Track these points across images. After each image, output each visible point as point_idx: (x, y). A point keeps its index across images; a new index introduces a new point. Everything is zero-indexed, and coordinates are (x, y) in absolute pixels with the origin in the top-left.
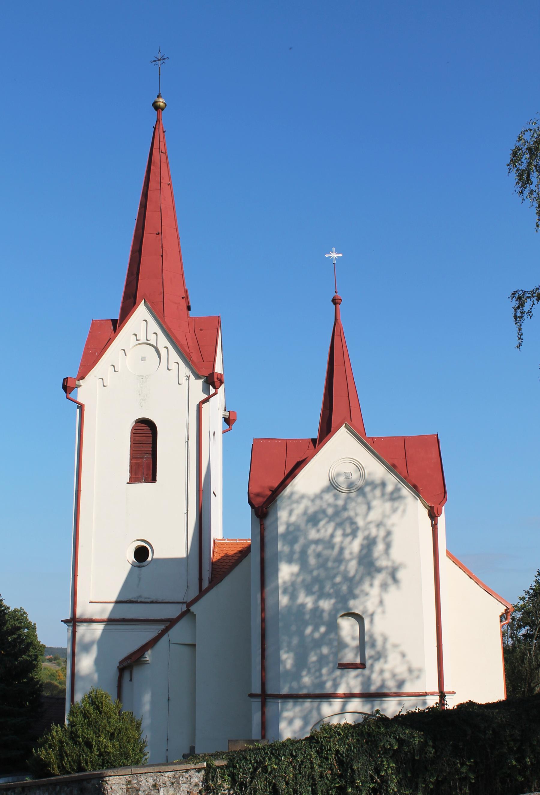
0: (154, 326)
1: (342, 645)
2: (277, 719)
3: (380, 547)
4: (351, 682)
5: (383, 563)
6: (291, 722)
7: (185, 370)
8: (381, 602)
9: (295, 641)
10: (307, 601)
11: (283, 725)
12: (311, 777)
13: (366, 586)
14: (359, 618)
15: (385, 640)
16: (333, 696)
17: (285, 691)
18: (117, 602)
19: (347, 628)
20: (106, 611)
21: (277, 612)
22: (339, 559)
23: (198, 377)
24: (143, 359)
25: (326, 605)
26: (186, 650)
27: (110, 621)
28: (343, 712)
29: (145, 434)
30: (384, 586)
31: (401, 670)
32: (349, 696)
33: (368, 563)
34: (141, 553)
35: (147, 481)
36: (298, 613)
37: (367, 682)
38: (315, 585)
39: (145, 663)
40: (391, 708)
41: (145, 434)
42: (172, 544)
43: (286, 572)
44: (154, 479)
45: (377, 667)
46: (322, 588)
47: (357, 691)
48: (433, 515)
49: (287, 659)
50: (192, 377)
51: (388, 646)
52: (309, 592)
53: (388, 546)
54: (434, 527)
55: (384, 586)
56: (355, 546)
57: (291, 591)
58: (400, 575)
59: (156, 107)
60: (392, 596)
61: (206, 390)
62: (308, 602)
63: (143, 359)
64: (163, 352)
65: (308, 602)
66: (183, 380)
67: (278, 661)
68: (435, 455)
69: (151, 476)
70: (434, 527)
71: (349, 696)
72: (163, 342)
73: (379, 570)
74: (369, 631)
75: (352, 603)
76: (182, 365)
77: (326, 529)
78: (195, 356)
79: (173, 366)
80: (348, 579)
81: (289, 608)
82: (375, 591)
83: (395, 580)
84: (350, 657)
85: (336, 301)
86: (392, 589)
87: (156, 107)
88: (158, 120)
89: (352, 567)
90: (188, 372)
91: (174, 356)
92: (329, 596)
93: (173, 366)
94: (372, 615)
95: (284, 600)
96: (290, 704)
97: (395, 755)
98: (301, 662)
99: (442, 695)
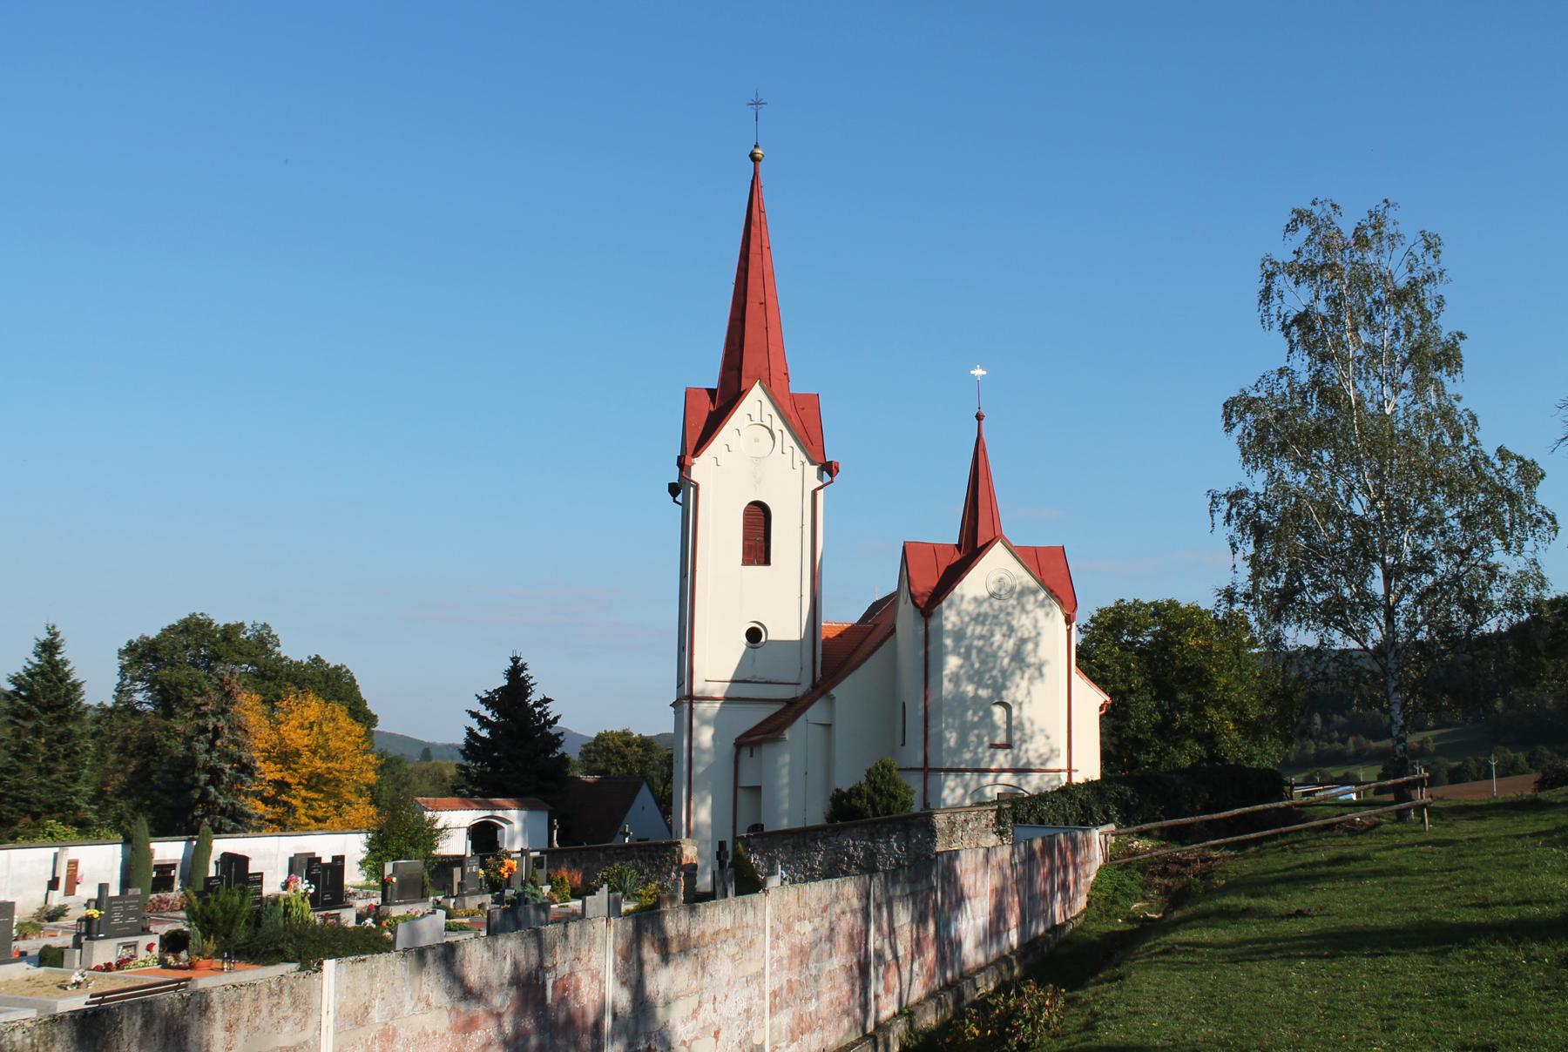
0: (768, 408)
1: (994, 727)
2: (940, 788)
3: (1030, 646)
4: (1002, 759)
5: (1031, 659)
6: (953, 790)
7: (800, 456)
8: (1029, 693)
9: (957, 723)
11: (946, 793)
12: (1064, 816)
13: (1017, 678)
14: (1007, 707)
15: (1032, 724)
16: (988, 771)
17: (948, 765)
18: (732, 681)
19: (999, 713)
20: (719, 690)
22: (994, 655)
23: (813, 463)
24: (757, 441)
25: (983, 693)
26: (820, 729)
27: (727, 699)
28: (995, 783)
29: (758, 519)
30: (1031, 679)
31: (1044, 750)
32: (1002, 771)
33: (1018, 657)
34: (754, 635)
35: (759, 564)
36: (960, 700)
37: (1016, 759)
38: (977, 678)
39: (783, 740)
40: (1033, 784)
41: (758, 519)
42: (786, 626)
43: (953, 663)
44: (767, 562)
45: (1024, 747)
46: (981, 679)
47: (1006, 766)
48: (1069, 621)
49: (952, 738)
50: (807, 463)
51: (1036, 728)
52: (970, 679)
53: (1037, 645)
54: (1069, 631)
55: (1031, 679)
56: (1010, 645)
57: (956, 679)
58: (1045, 670)
59: (754, 158)
60: (1038, 687)
61: (820, 477)
62: (970, 689)
63: (757, 441)
64: (778, 435)
65: (970, 689)
66: (798, 465)
67: (941, 739)
68: (1063, 564)
70: (1069, 631)
71: (1002, 771)
72: (778, 425)
73: (1029, 666)
74: (1019, 717)
75: (1004, 693)
76: (797, 449)
79: (788, 450)
80: (1003, 672)
82: (1024, 684)
83: (1041, 675)
84: (1001, 738)
85: (979, 417)
86: (1038, 682)
87: (754, 158)
88: (755, 174)
90: (804, 458)
91: (789, 440)
92: (987, 687)
93: (788, 450)
94: (1020, 704)
95: (947, 686)
96: (952, 776)
97: (1115, 802)
98: (963, 742)
99: (1070, 770)
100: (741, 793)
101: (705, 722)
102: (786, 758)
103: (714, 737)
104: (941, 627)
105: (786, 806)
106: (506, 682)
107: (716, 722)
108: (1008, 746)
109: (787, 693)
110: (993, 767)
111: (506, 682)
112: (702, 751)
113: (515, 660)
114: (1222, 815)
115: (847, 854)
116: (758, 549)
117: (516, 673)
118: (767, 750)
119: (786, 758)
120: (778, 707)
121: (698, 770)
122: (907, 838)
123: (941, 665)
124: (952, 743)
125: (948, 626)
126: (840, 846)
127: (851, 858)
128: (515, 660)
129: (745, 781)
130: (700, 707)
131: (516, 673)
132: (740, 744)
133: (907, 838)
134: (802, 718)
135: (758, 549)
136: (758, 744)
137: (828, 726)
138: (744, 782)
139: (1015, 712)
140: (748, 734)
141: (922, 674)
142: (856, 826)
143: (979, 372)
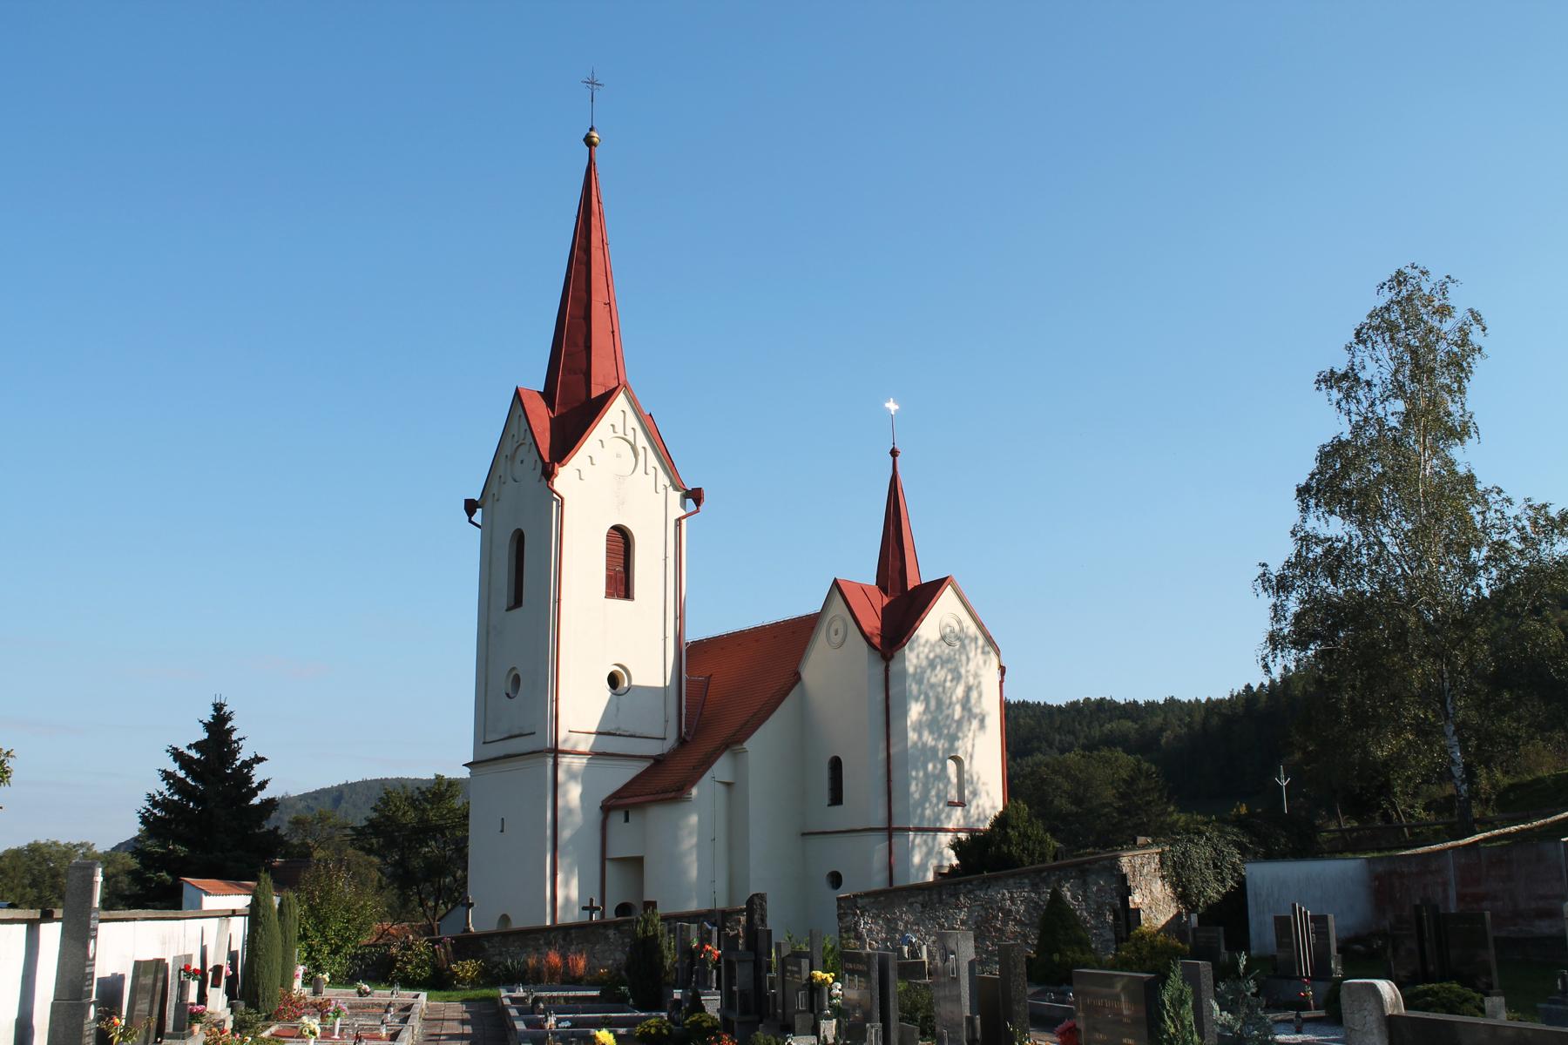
0: (632, 421)
5: (976, 710)
10: (928, 739)
18: (598, 733)
20: (585, 744)
21: (906, 749)
23: (676, 489)
24: (618, 456)
26: (722, 788)
29: (621, 542)
34: (613, 680)
35: (619, 597)
41: (621, 542)
42: (653, 669)
43: (915, 711)
45: (974, 804)
50: (670, 489)
56: (960, 691)
57: (919, 728)
61: (683, 505)
63: (618, 456)
64: (641, 452)
67: (907, 793)
69: (627, 594)
77: (940, 674)
78: (508, 451)
79: (651, 471)
81: (915, 744)
84: (953, 795)
85: (894, 453)
87: (589, 141)
89: (958, 712)
90: (668, 483)
93: (651, 471)
95: (912, 736)
100: (608, 864)
101: (572, 776)
102: (694, 819)
103: (583, 796)
104: (904, 671)
105: (693, 873)
106: (205, 736)
107: (586, 778)
108: (961, 804)
109: (655, 749)
110: (950, 826)
111: (205, 736)
112: (570, 811)
113: (218, 708)
114: (1420, 850)
115: (1001, 909)
116: (621, 583)
117: (219, 726)
118: (658, 816)
119: (694, 819)
120: (645, 765)
121: (565, 834)
122: (1085, 885)
123: (905, 713)
124: (917, 796)
125: (911, 670)
126: (992, 900)
127: (1008, 913)
128: (218, 708)
129: (615, 851)
130: (565, 761)
131: (219, 726)
132: (607, 808)
133: (1085, 885)
134: (707, 777)
135: (621, 583)
136: (640, 806)
137: (728, 784)
138: (615, 851)
139: (967, 766)
140: (617, 795)
141: (883, 718)
142: (1013, 876)
143: (892, 406)
